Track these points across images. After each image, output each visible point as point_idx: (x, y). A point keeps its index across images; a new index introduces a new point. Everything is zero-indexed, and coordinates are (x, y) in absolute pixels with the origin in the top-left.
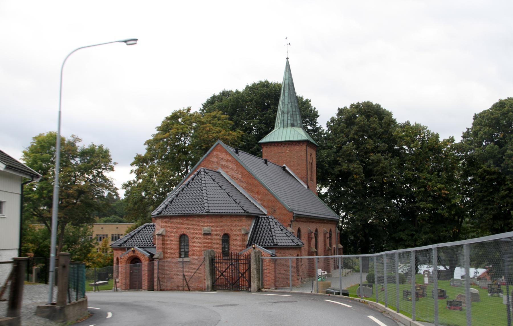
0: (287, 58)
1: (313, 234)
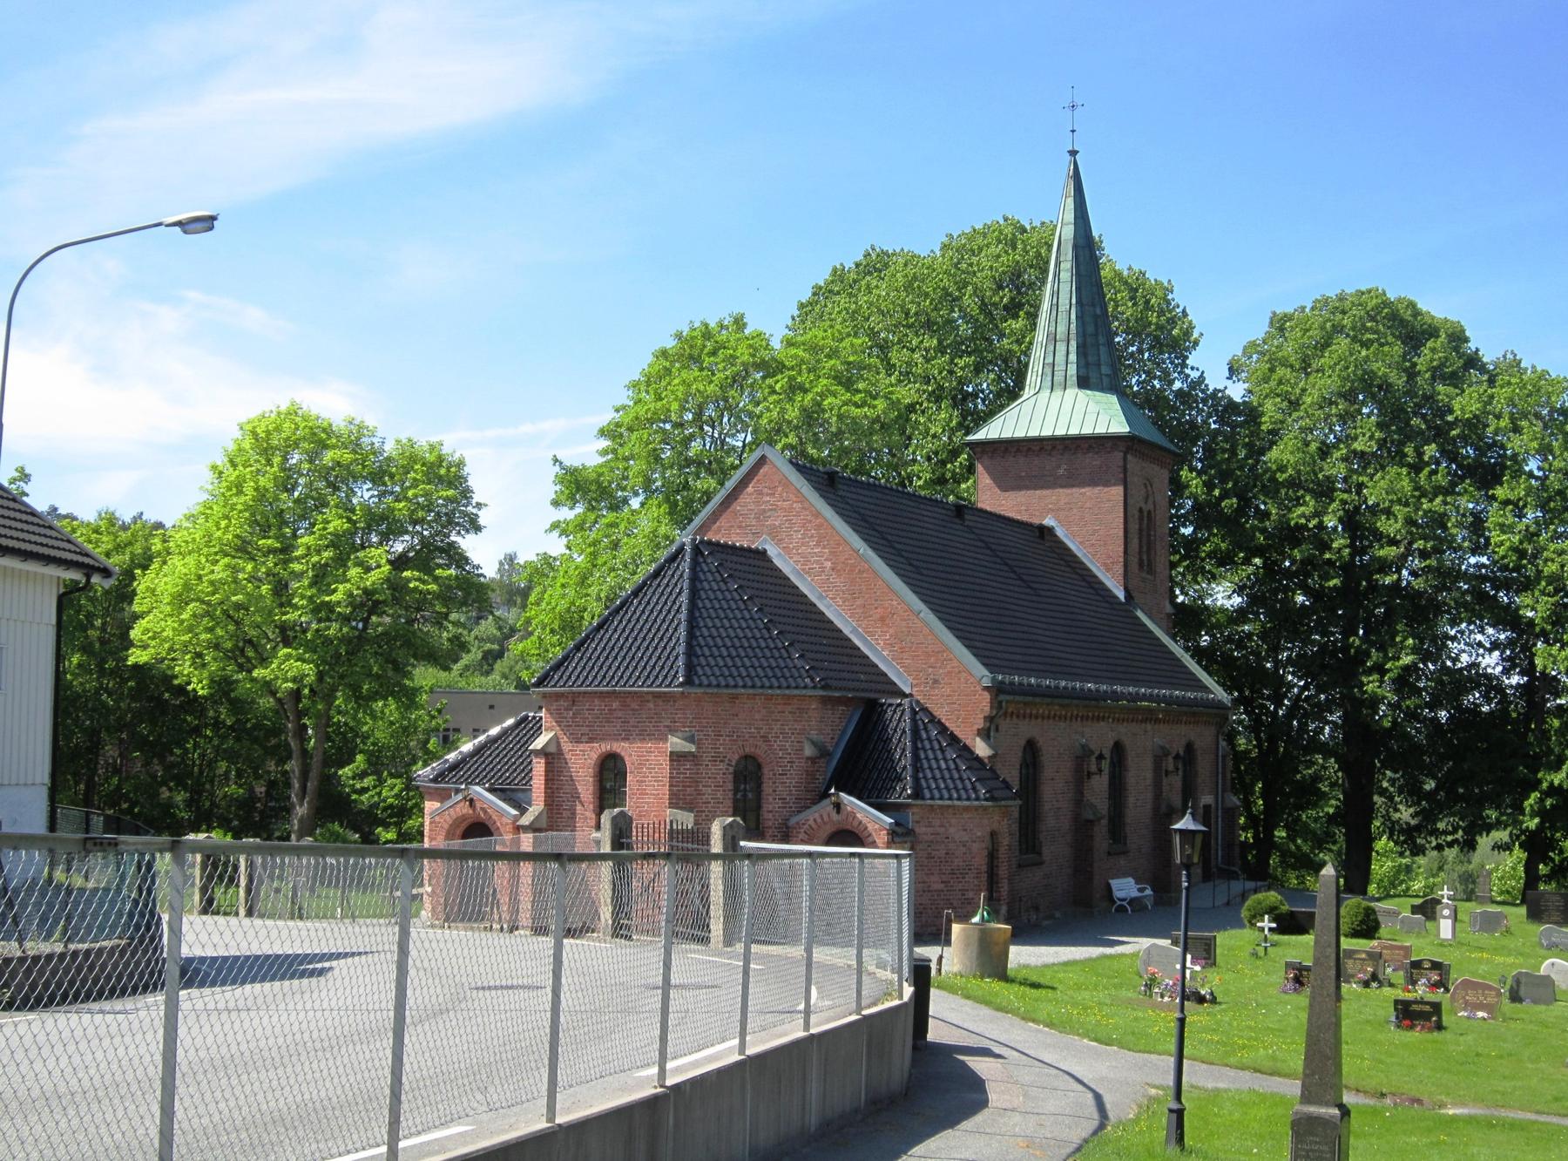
0: (1073, 153)
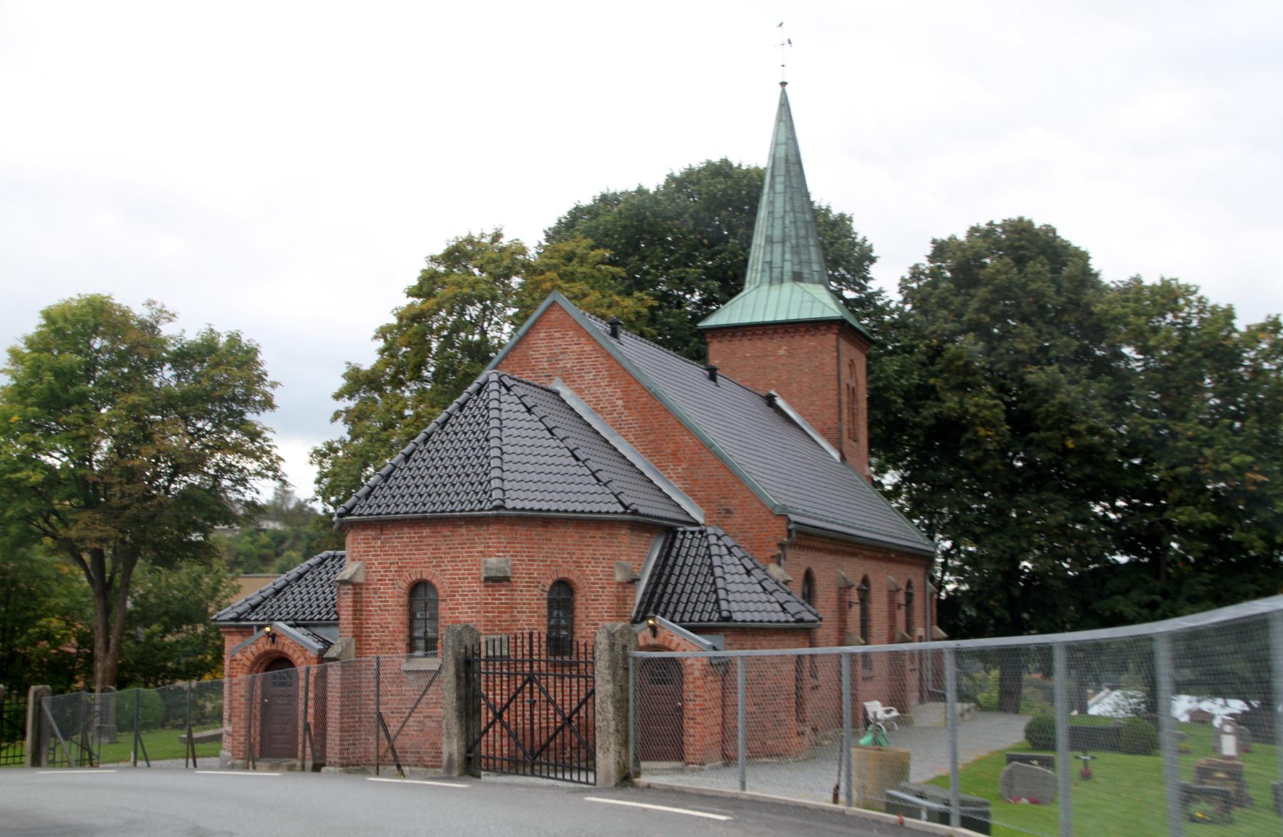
0: (783, 84)
1: (854, 590)
